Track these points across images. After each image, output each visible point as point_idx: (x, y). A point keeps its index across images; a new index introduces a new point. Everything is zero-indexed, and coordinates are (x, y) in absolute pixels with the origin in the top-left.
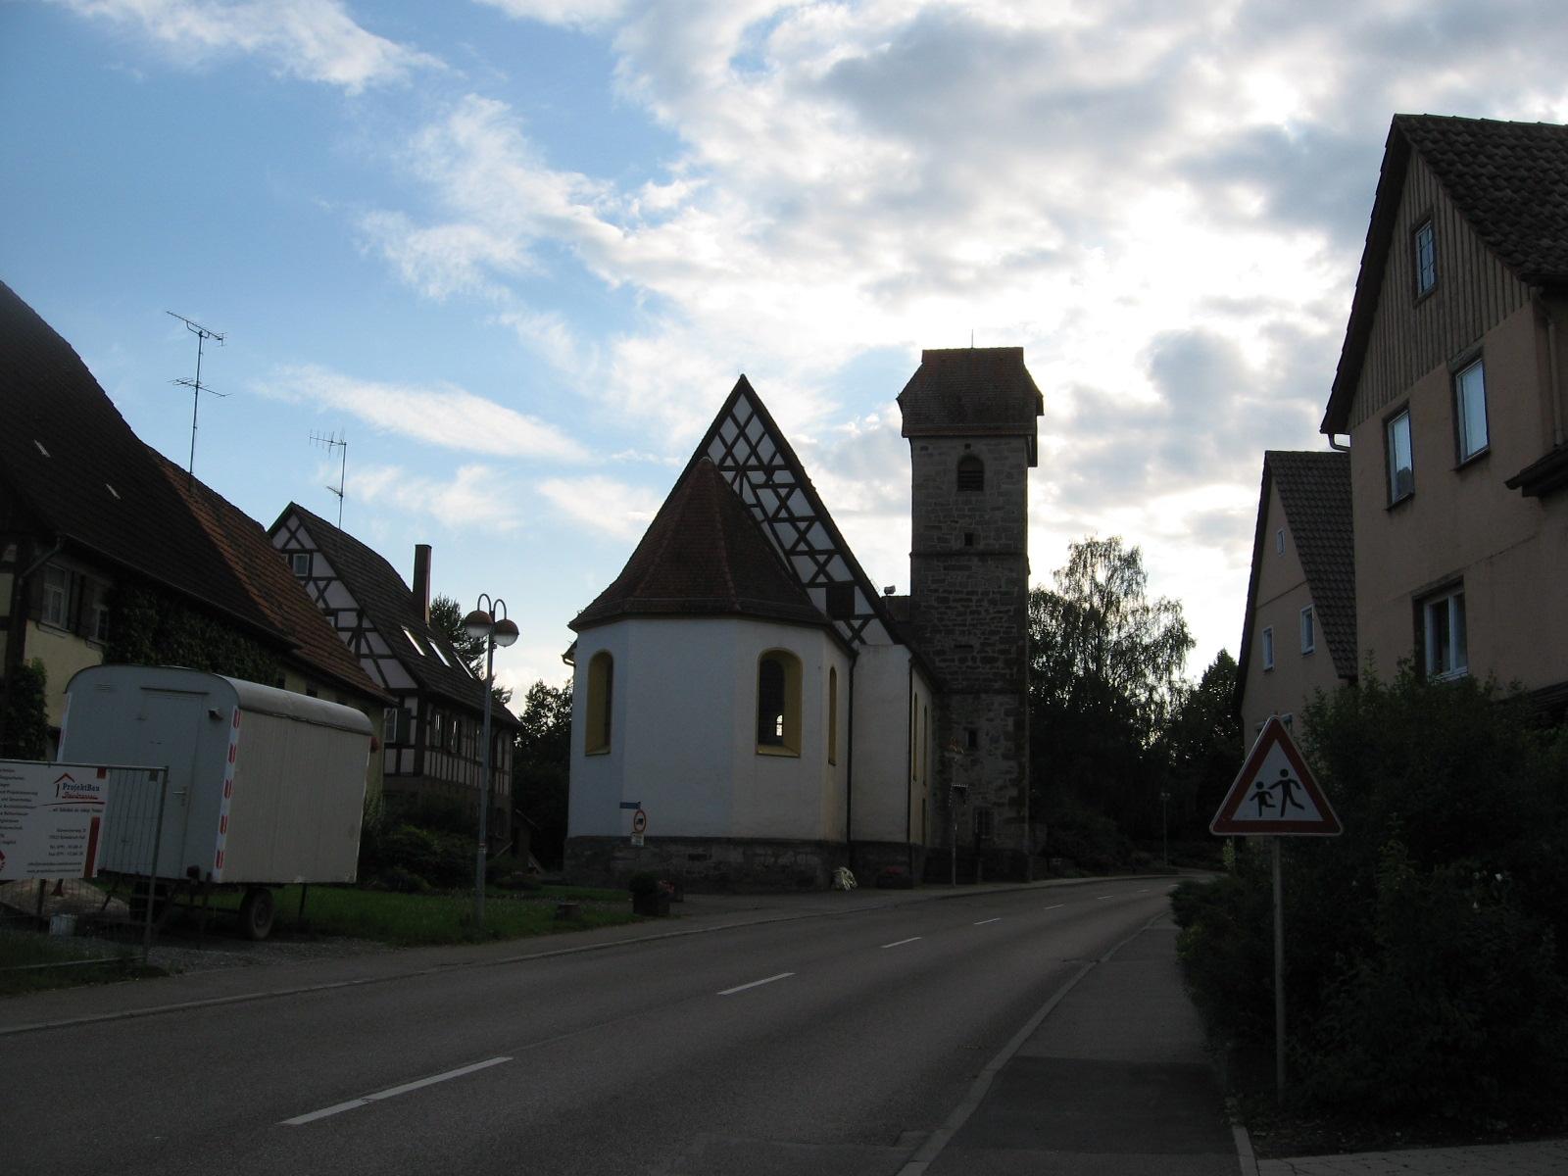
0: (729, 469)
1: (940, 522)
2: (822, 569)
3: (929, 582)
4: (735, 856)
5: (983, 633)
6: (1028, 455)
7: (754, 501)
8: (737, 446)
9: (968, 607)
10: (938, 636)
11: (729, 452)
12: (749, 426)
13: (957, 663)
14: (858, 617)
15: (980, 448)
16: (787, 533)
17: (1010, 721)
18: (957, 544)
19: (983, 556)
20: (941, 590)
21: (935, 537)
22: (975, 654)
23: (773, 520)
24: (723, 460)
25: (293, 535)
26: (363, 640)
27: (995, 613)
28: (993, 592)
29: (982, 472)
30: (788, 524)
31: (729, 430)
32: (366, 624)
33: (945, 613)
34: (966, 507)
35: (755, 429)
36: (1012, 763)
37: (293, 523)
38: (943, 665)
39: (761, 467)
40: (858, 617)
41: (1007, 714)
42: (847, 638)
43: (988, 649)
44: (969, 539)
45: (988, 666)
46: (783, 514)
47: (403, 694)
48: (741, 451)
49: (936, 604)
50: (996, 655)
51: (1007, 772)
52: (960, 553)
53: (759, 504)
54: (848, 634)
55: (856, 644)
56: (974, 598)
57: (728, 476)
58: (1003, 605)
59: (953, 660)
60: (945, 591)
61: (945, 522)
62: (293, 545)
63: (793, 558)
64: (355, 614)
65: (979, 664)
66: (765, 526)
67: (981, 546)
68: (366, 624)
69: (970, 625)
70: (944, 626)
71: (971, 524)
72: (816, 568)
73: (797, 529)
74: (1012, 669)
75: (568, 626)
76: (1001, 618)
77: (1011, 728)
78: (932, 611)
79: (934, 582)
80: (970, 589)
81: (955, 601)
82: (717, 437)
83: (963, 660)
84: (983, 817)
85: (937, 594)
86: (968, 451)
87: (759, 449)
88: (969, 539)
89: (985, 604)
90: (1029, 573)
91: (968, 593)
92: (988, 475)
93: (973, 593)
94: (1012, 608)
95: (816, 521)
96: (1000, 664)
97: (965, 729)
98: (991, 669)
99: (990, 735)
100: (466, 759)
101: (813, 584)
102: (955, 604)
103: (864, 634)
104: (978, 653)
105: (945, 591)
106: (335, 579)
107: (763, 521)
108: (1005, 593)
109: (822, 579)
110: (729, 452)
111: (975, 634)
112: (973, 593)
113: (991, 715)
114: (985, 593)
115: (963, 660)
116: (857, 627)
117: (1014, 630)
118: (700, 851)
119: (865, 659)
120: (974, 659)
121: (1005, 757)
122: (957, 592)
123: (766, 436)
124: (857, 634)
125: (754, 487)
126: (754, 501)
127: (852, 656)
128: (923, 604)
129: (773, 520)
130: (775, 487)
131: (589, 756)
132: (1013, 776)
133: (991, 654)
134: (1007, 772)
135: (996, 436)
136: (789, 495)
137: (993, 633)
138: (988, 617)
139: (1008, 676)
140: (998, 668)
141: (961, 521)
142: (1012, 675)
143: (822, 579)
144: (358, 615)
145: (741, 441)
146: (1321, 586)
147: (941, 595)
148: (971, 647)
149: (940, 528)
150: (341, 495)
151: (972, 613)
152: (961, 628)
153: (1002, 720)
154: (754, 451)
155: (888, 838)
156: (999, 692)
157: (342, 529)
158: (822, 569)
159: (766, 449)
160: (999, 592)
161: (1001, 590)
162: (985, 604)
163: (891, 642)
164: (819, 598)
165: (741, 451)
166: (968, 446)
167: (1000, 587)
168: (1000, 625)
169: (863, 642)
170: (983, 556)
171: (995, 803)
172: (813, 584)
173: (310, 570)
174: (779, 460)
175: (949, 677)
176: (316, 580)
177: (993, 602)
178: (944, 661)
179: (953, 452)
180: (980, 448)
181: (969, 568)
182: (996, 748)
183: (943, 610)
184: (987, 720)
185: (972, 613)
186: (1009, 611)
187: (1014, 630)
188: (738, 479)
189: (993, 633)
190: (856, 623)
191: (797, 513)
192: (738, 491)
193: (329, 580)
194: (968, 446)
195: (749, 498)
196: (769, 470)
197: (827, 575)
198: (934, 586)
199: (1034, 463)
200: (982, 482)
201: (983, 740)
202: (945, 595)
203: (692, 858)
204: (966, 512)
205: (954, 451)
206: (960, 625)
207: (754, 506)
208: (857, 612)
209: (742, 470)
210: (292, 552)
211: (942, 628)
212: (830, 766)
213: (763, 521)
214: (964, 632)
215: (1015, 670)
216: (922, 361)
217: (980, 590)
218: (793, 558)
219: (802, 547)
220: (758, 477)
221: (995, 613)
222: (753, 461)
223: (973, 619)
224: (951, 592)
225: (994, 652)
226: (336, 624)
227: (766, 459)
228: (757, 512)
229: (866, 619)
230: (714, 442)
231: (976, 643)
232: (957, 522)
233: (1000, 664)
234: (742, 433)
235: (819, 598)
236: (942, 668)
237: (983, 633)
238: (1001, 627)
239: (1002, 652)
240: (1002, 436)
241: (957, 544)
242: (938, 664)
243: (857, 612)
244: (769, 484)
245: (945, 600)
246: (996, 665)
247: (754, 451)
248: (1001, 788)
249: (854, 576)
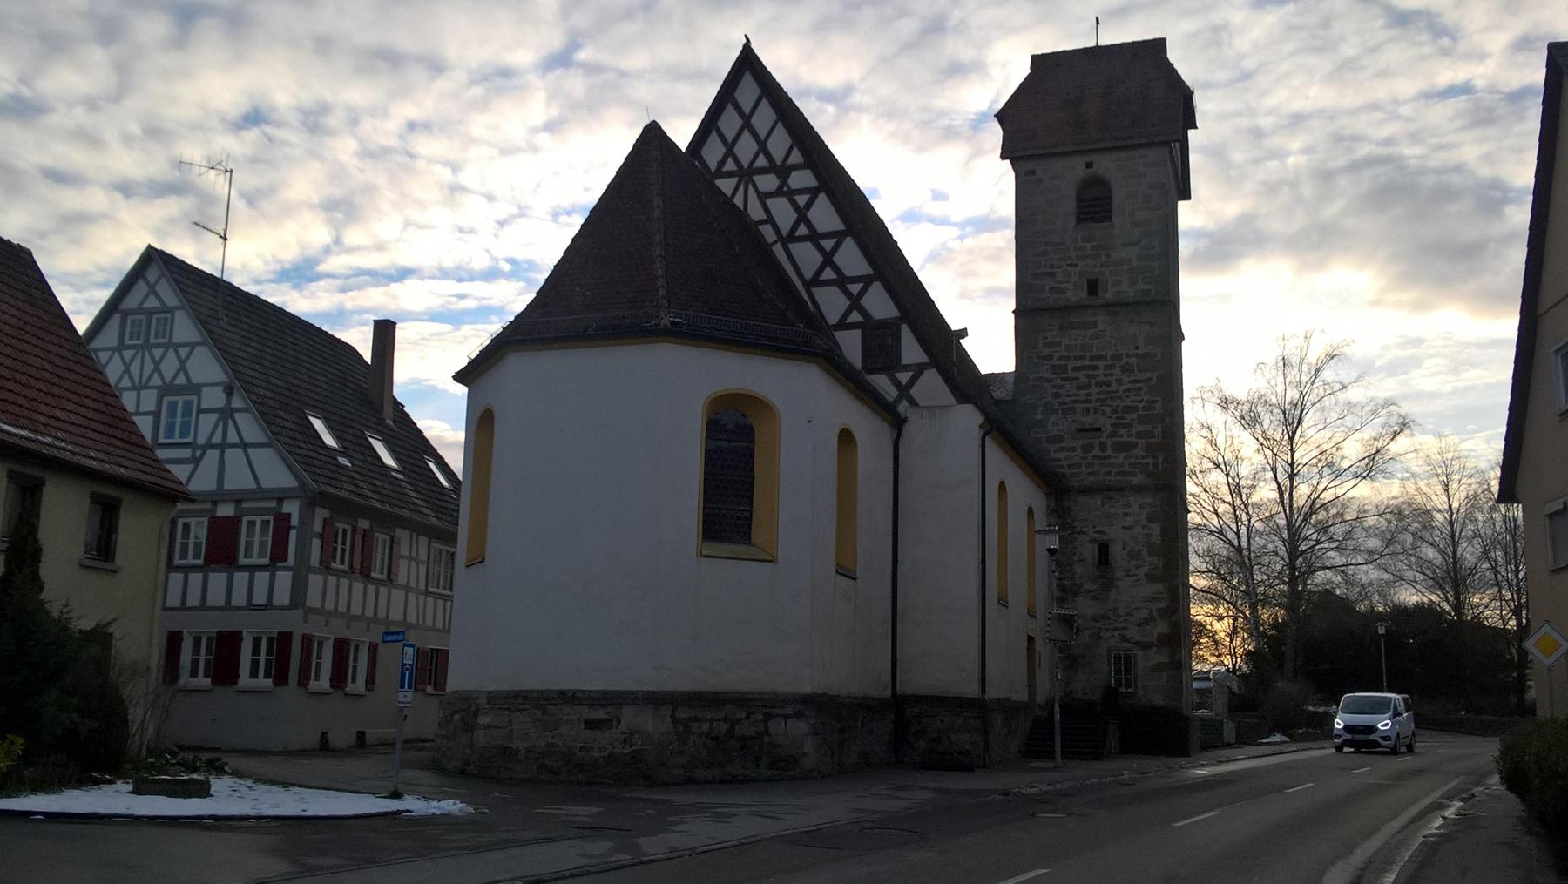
0: (730, 174)
1: (1052, 266)
2: (855, 303)
3: (1040, 345)
4: (652, 724)
5: (1114, 411)
6: (1175, 171)
7: (762, 216)
8: (740, 142)
9: (1094, 376)
10: (1053, 418)
11: (730, 152)
12: (755, 116)
13: (1079, 451)
14: (906, 368)
15: (1106, 165)
16: (807, 256)
17: (1156, 528)
18: (1075, 294)
19: (1114, 307)
20: (1055, 357)
21: (1047, 288)
22: (1103, 439)
23: (788, 239)
24: (722, 162)
25: (152, 290)
26: (230, 421)
27: (1131, 382)
28: (1128, 356)
29: (1109, 198)
30: (809, 244)
31: (730, 122)
32: (237, 402)
33: (1063, 386)
34: (1088, 245)
35: (764, 118)
36: (1159, 587)
37: (152, 273)
38: (1062, 455)
39: (772, 168)
40: (906, 368)
41: (1151, 519)
42: (890, 399)
43: (1122, 431)
44: (1093, 287)
45: (1123, 455)
46: (802, 230)
47: (281, 496)
48: (746, 149)
49: (1049, 376)
50: (1134, 440)
51: (1154, 599)
52: (1078, 308)
53: (770, 220)
54: (891, 392)
55: (903, 407)
56: (1101, 364)
57: (726, 185)
58: (1141, 371)
59: (1073, 449)
60: (1060, 358)
61: (1059, 267)
62: (152, 303)
63: (816, 291)
64: (220, 389)
65: (1109, 452)
66: (778, 250)
67: (1109, 295)
68: (237, 402)
69: (1097, 400)
70: (1061, 403)
71: (1095, 266)
72: (848, 303)
73: (820, 249)
74: (1157, 458)
75: (454, 377)
76: (1140, 389)
77: (1156, 538)
78: (1045, 384)
79: (1047, 345)
80: (1095, 353)
81: (1075, 369)
82: (714, 132)
83: (1087, 448)
84: (1124, 663)
85: (1050, 362)
86: (1090, 170)
87: (769, 144)
88: (1093, 287)
89: (1117, 370)
90: (1182, 338)
91: (1093, 358)
92: (1117, 199)
93: (1099, 358)
94: (1154, 376)
95: (847, 236)
96: (1139, 451)
97: (1093, 541)
98: (1126, 458)
99: (1128, 549)
100: (407, 589)
101: (842, 325)
102: (1075, 374)
103: (915, 392)
104: (1108, 437)
105: (1060, 358)
106: (199, 344)
107: (775, 242)
108: (1144, 356)
109: (855, 317)
110: (730, 152)
111: (1104, 412)
112: (1099, 358)
113: (1129, 521)
114: (1118, 357)
115: (1087, 448)
116: (904, 382)
117: (1159, 405)
118: (599, 714)
119: (917, 427)
120: (1103, 447)
121: (1151, 578)
122: (1078, 358)
123: (780, 125)
124: (904, 390)
125: (763, 197)
126: (762, 216)
127: (898, 423)
128: (1032, 376)
129: (788, 239)
130: (791, 194)
131: (468, 566)
132: (1163, 605)
133: (1125, 439)
134: (1154, 599)
135: (1127, 148)
136: (809, 205)
137: (1128, 409)
138: (1122, 389)
139: (1151, 468)
140: (1137, 457)
141: (1080, 264)
142: (1156, 465)
143: (855, 317)
144: (224, 391)
145: (746, 136)
146: (1461, 488)
147: (1056, 363)
148: (1099, 429)
149: (1052, 275)
150: (225, 239)
151: (1099, 384)
152: (1085, 405)
153: (1144, 527)
154: (763, 148)
155: (953, 691)
156: (1140, 489)
157: (224, 278)
158: (855, 303)
159: (779, 143)
160: (1137, 356)
161: (1140, 351)
162: (1117, 370)
163: (953, 401)
164: (851, 345)
165: (746, 149)
166: (1089, 165)
167: (1137, 348)
168: (1139, 398)
169: (913, 403)
170: (1114, 307)
171: (1137, 644)
172: (842, 325)
173: (171, 335)
174: (796, 157)
175: (1067, 471)
176: (176, 347)
177: (1127, 369)
178: (1061, 449)
179: (1068, 174)
180: (1106, 165)
181: (1095, 325)
182: (1137, 567)
183: (1059, 382)
184: (1124, 527)
185: (1099, 384)
186: (1151, 379)
187: (1159, 405)
188: (742, 188)
189: (1128, 409)
190: (904, 377)
191: (821, 227)
192: (741, 206)
193: (193, 346)
194: (1089, 165)
195: (755, 212)
196: (783, 171)
197: (863, 312)
198: (1046, 352)
199: (1186, 195)
200: (1110, 211)
201: (1118, 555)
202: (1063, 363)
203: (591, 724)
204: (1089, 252)
205: (1069, 173)
206: (1083, 402)
207: (762, 222)
208: (904, 361)
209: (746, 175)
210: (150, 313)
211: (1057, 406)
212: (842, 580)
213: (775, 242)
214: (1088, 409)
215: (1161, 459)
216: (1031, 68)
217: (1110, 354)
218: (816, 291)
219: (828, 274)
220: (768, 182)
221: (1131, 382)
222: (761, 162)
223: (1098, 394)
224: (1069, 358)
225: (1130, 435)
226: (199, 404)
227: (778, 157)
228: (768, 232)
229: (919, 370)
230: (711, 137)
231: (1106, 424)
232: (1076, 265)
233: (1139, 451)
234: (747, 125)
235: (851, 345)
236: (1059, 460)
237: (1114, 411)
238: (1141, 401)
239: (1140, 435)
240: (1135, 147)
241: (1075, 294)
242: (1053, 455)
243: (904, 361)
244: (783, 191)
245: (1057, 370)
246: (1133, 452)
247: (763, 148)
248: (1146, 621)
249: (819, 243)
